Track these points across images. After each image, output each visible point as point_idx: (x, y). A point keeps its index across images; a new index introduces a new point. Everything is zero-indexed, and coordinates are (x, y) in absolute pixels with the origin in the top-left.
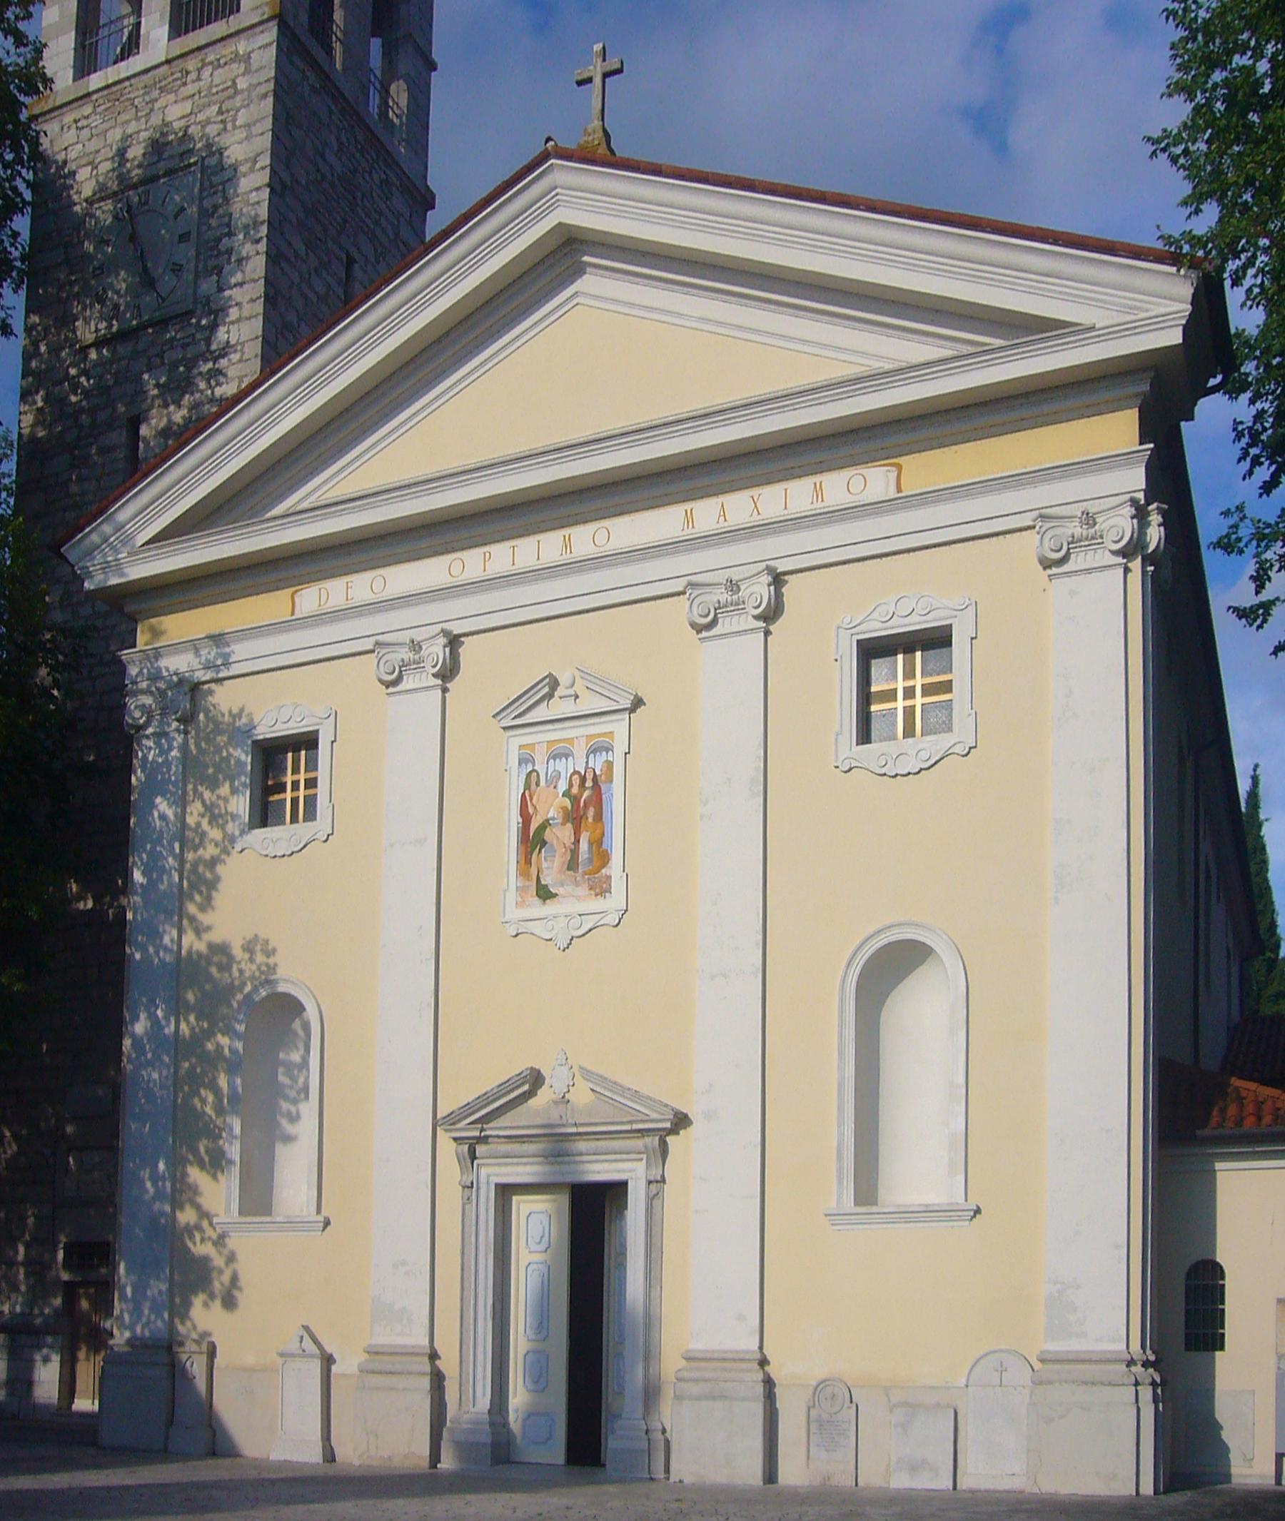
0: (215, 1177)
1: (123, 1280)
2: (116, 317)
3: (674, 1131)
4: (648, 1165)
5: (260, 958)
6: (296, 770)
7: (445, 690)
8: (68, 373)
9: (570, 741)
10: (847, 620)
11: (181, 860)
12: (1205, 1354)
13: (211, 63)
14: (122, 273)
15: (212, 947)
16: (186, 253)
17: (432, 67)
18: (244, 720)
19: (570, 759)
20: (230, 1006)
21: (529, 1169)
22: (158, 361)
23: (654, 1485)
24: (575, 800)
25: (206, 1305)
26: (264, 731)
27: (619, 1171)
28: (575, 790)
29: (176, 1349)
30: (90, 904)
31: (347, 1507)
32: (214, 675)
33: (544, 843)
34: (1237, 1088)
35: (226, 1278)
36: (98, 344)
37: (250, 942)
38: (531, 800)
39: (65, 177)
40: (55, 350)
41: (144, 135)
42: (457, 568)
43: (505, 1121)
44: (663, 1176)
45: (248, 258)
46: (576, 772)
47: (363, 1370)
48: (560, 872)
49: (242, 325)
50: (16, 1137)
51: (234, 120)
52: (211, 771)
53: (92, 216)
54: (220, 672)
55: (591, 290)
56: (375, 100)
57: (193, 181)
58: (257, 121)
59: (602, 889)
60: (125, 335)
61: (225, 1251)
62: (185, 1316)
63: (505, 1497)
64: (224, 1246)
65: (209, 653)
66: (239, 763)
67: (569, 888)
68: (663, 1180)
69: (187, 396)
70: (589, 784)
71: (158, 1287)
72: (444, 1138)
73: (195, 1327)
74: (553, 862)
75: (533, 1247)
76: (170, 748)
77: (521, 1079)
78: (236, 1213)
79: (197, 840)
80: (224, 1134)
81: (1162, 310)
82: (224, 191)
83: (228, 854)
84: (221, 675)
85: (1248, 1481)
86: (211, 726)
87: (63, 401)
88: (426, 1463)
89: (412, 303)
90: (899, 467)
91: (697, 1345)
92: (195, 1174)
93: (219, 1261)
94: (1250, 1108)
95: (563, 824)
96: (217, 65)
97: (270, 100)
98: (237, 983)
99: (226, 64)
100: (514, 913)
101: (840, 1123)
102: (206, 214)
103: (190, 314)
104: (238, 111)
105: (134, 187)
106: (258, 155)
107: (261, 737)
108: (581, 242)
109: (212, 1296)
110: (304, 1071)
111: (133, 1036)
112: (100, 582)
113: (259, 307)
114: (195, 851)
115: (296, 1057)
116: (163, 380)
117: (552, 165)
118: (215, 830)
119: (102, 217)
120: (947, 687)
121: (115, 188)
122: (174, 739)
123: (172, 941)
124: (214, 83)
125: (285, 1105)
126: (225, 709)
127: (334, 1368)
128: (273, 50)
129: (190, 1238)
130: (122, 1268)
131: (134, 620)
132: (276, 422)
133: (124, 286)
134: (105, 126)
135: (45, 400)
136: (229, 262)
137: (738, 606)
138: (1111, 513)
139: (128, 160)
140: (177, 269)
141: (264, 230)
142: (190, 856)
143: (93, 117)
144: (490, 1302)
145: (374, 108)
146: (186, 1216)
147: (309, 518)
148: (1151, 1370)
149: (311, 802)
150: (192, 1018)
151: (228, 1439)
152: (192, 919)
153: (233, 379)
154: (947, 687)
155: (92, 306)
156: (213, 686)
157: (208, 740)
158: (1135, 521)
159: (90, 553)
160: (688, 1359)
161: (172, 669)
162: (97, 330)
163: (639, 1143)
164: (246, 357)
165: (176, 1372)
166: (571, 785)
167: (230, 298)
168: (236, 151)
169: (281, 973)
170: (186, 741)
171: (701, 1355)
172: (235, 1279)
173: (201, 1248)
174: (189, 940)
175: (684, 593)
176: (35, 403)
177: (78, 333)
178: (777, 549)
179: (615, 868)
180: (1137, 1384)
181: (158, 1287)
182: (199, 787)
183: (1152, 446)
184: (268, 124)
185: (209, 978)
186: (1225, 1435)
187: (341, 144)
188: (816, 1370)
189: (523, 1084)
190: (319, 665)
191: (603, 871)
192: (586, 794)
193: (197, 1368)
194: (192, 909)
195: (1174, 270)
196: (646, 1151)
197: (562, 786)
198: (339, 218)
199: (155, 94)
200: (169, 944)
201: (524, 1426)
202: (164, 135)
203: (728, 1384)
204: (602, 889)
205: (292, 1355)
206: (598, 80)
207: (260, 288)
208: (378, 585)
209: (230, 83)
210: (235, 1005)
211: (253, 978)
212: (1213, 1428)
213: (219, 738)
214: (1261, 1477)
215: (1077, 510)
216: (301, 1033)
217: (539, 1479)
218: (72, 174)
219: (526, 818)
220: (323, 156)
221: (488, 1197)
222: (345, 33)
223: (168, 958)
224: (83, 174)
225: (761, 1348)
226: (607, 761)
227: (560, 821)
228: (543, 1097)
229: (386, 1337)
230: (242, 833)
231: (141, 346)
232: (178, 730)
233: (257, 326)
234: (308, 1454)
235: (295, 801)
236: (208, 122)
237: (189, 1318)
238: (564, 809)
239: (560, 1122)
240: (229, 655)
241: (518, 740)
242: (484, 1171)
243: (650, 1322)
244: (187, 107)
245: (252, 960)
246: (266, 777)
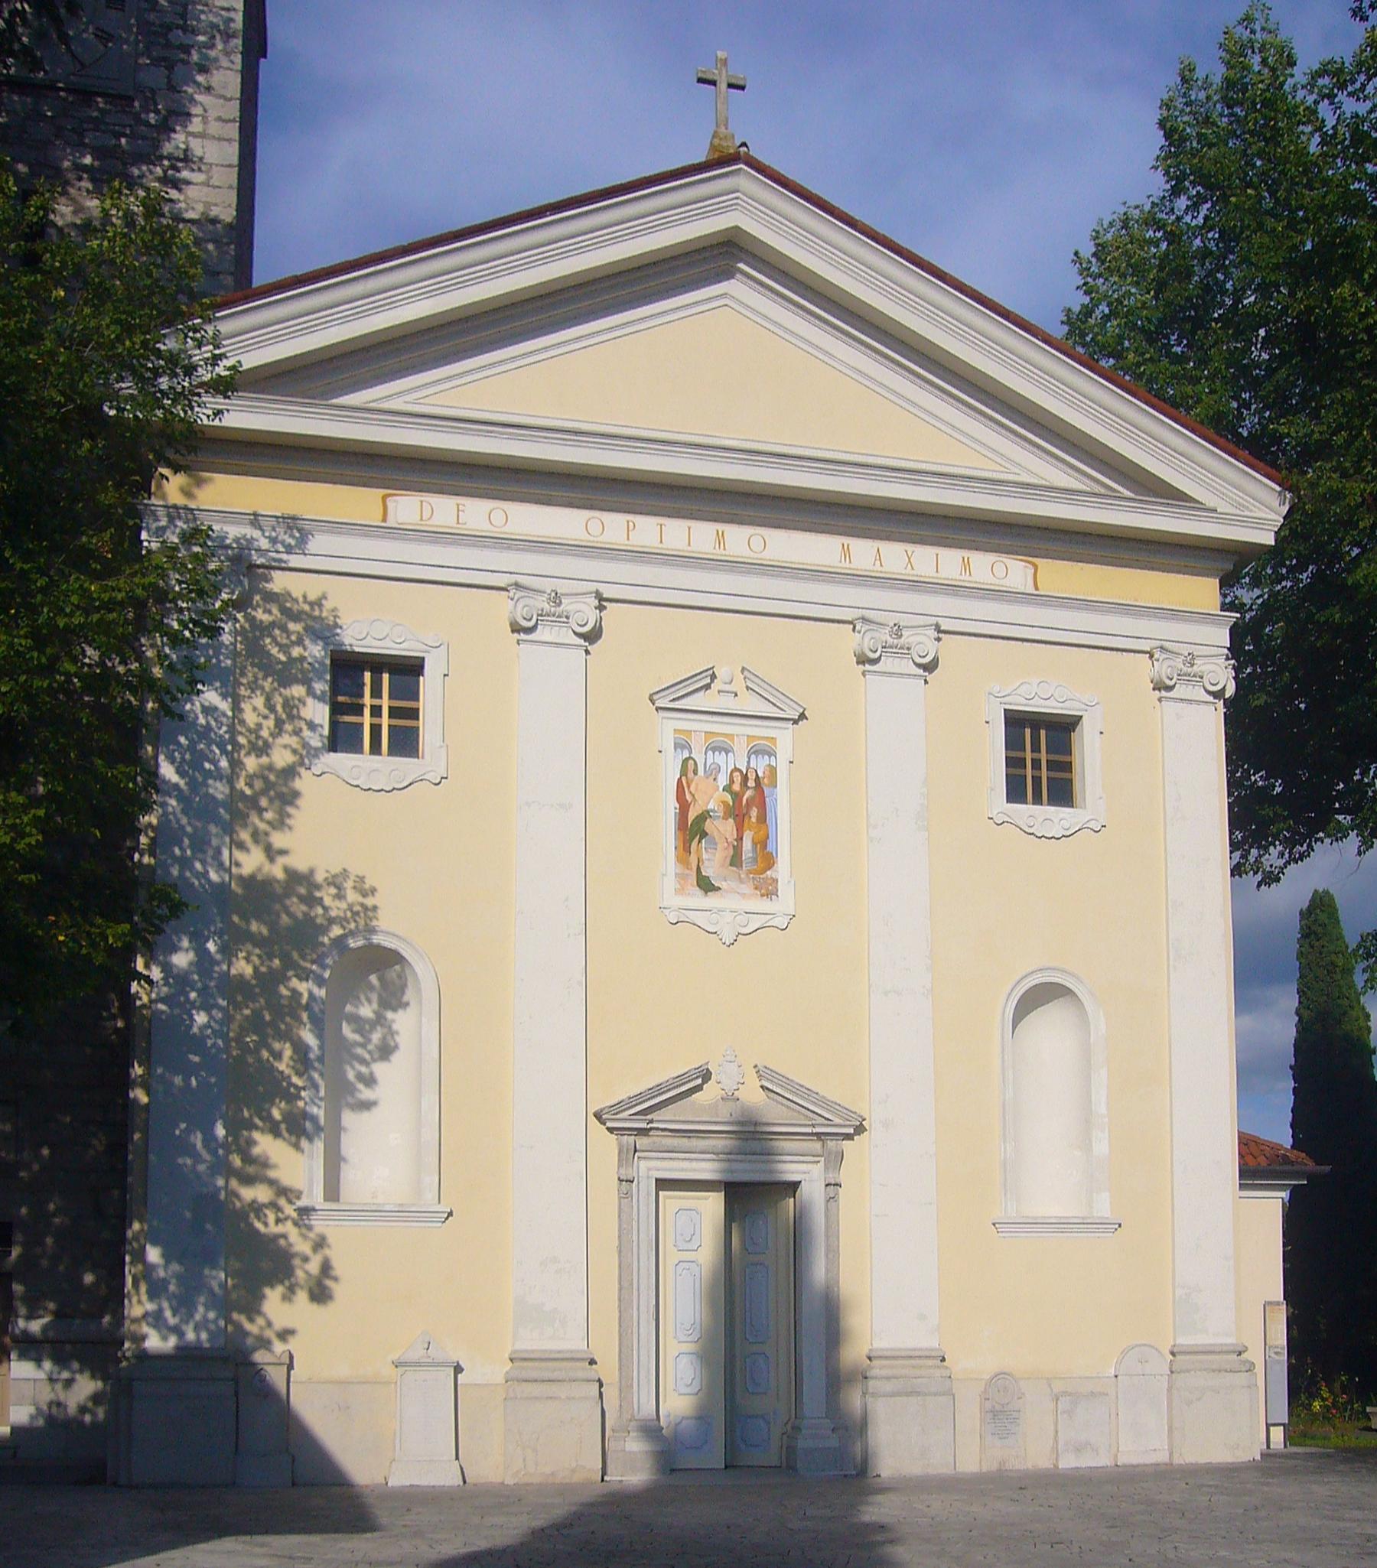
0: (297, 1146)
4: (826, 1168)
5: (352, 896)
9: (731, 736)
15: (295, 877)
19: (730, 754)
24: (736, 797)
28: (736, 787)
33: (704, 834)
35: (314, 1267)
38: (689, 787)
46: (736, 769)
48: (723, 866)
59: (769, 890)
64: (310, 1228)
67: (733, 884)
70: (751, 783)
73: (269, 1324)
74: (714, 854)
81: (1264, 516)
89: (903, 292)
92: (265, 1144)
95: (725, 818)
108: (741, 249)
117: (740, 169)
129: (259, 1219)
132: (392, 305)
138: (919, 630)
147: (447, 427)
164: (214, 182)
166: (732, 781)
171: (888, 1354)
172: (326, 1268)
179: (782, 871)
183: (1238, 615)
189: (697, 1078)
190: (796, 621)
191: (768, 873)
192: (748, 794)
195: (1278, 488)
197: (723, 780)
203: (919, 1380)
204: (769, 890)
215: (1185, 650)
219: (684, 806)
228: (710, 1093)
229: (533, 1341)
237: (259, 1312)
238: (725, 803)
241: (668, 727)
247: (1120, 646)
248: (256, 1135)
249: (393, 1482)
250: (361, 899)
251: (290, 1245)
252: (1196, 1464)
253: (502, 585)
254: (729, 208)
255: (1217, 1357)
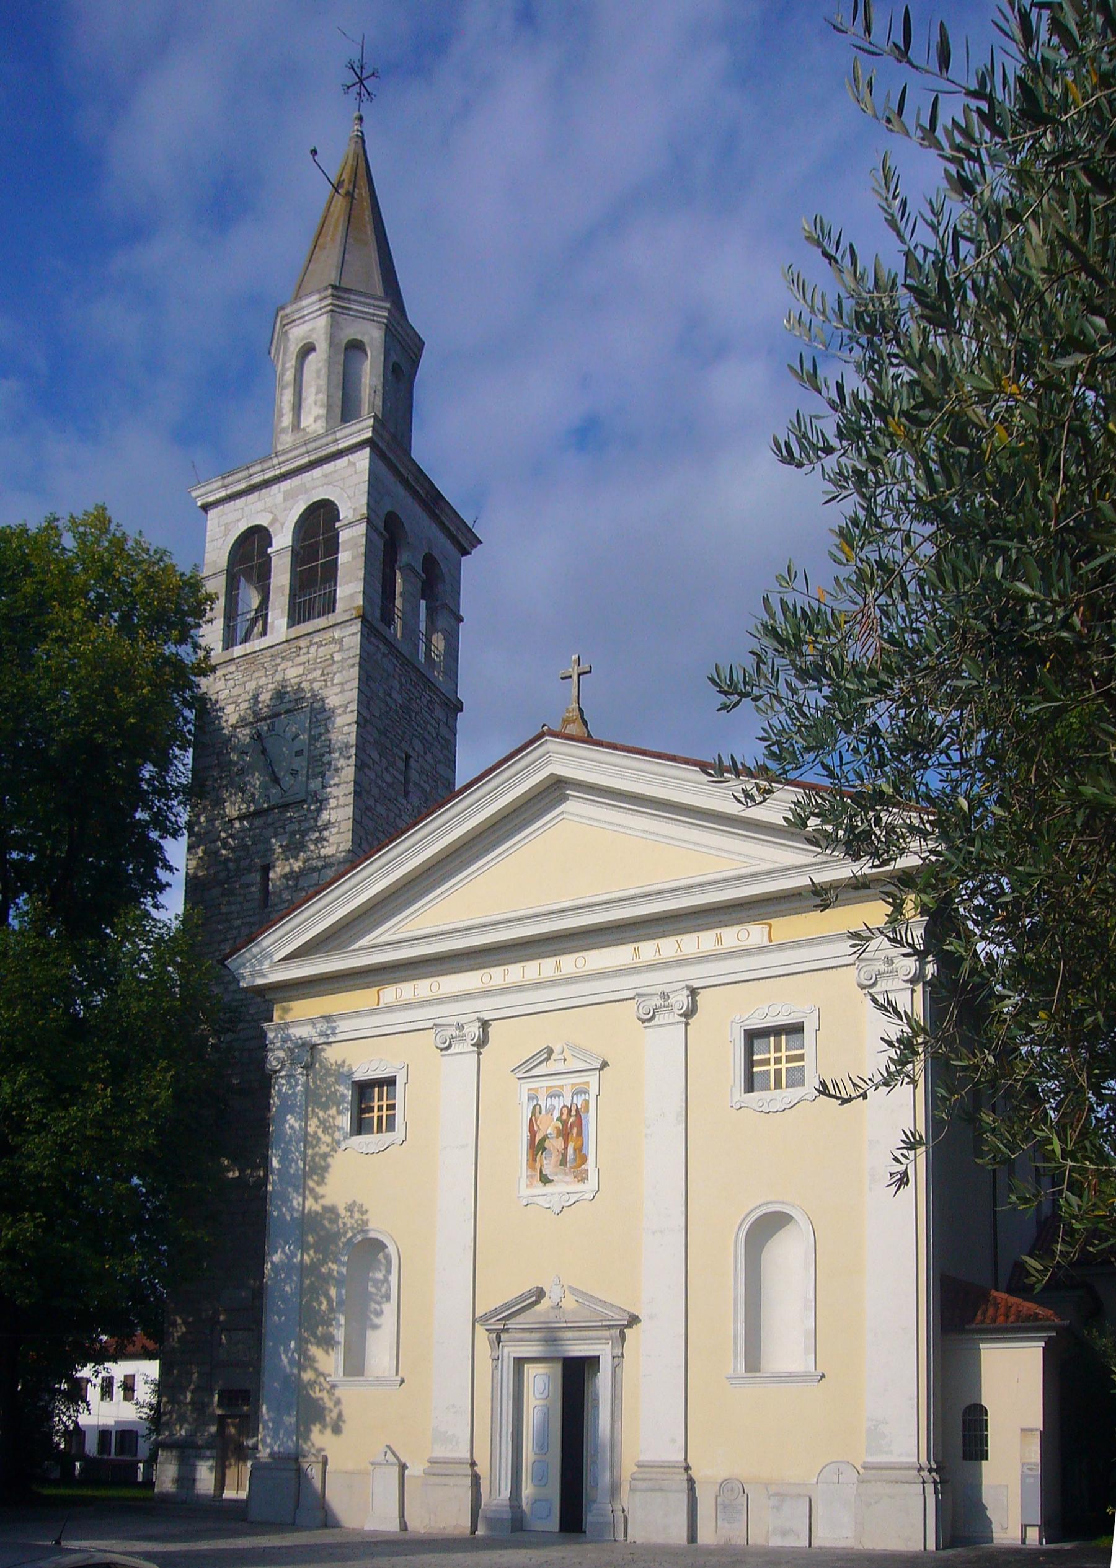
0: (327, 1352)
1: (266, 1417)
2: (253, 801)
3: (629, 1325)
4: (613, 1347)
5: (357, 1216)
6: (380, 1099)
7: (479, 1054)
8: (219, 836)
9: (561, 1087)
10: (738, 1018)
11: (305, 1153)
12: (973, 1462)
13: (316, 643)
14: (257, 774)
15: (324, 1207)
16: (300, 763)
17: (460, 619)
18: (346, 1069)
20: (337, 1246)
21: (535, 1348)
22: (282, 830)
23: (617, 1544)
24: (564, 1123)
25: (321, 1432)
26: (359, 1076)
27: (594, 1350)
28: (564, 1117)
29: (301, 1460)
30: (237, 1174)
31: (383, 1562)
32: (326, 1040)
33: (544, 1149)
34: (995, 1298)
35: (334, 1415)
36: (241, 818)
37: (350, 1205)
39: (217, 711)
40: (211, 821)
41: (271, 686)
42: (486, 979)
43: (521, 1318)
44: (622, 1354)
45: (342, 768)
46: (564, 1106)
47: (427, 1473)
49: (338, 810)
50: (185, 1322)
51: (332, 680)
52: (324, 1099)
53: (236, 737)
54: (330, 1037)
55: (571, 810)
56: (422, 647)
57: (304, 718)
58: (347, 682)
59: (583, 1178)
60: (258, 813)
61: (334, 1398)
62: (307, 1438)
63: (523, 1552)
64: (333, 1394)
65: (322, 1026)
66: (343, 1096)
68: (622, 1356)
69: (302, 854)
70: (573, 1113)
71: (290, 1420)
72: (480, 1331)
73: (313, 1445)
75: (538, 1396)
76: (297, 1085)
77: (531, 1293)
78: (342, 1374)
79: (314, 1142)
80: (334, 1323)
82: (326, 725)
83: (336, 1151)
84: (330, 1040)
85: (1004, 1542)
86: (324, 1071)
87: (217, 853)
88: (468, 1531)
90: (770, 926)
91: (646, 1457)
92: (314, 1350)
93: (329, 1404)
94: (1002, 1310)
95: (557, 1137)
96: (320, 644)
97: (357, 668)
98: (341, 1231)
99: (326, 644)
100: (525, 1191)
101: (735, 1321)
102: (313, 739)
103: (304, 801)
104: (335, 674)
105: (265, 719)
106: (349, 703)
107: (357, 1079)
108: (566, 783)
109: (324, 1426)
110: (385, 1285)
111: (273, 1263)
112: (249, 982)
113: (350, 799)
114: (313, 1149)
115: (380, 1276)
116: (284, 844)
118: (327, 1136)
119: (243, 738)
120: (801, 1057)
121: (251, 720)
122: (299, 1079)
123: (299, 1204)
124: (319, 656)
125: (373, 1306)
126: (333, 1061)
127: (407, 1472)
128: (359, 636)
130: (264, 1408)
131: (272, 1002)
132: (366, 889)
133: (258, 782)
134: (245, 679)
135: (204, 852)
136: (329, 770)
137: (669, 1008)
139: (259, 702)
140: (294, 773)
141: (353, 751)
142: (310, 1152)
143: (236, 674)
144: (510, 1430)
145: (422, 658)
146: (308, 1376)
148: (934, 1474)
149: (391, 1119)
150: (312, 1252)
151: (334, 1516)
152: (312, 1190)
153: (333, 844)
154: (801, 1057)
155: (236, 794)
156: (324, 1046)
157: (322, 1080)
158: (917, 963)
159: (243, 965)
160: (639, 1466)
161: (298, 1036)
162: (240, 809)
163: (607, 1333)
164: (341, 831)
165: (300, 1474)
166: (562, 1114)
167: (330, 793)
168: (333, 700)
169: (371, 1226)
170: (307, 1081)
171: (647, 1464)
172: (340, 1415)
173: (316, 1394)
174: (310, 1203)
175: (634, 998)
176: (197, 854)
177: (227, 810)
178: (695, 974)
180: (924, 1482)
181: (290, 1420)
182: (316, 1110)
183: (927, 918)
184: (356, 684)
185: (324, 1227)
186: (989, 1513)
187: (402, 685)
188: (721, 1472)
192: (572, 1119)
193: (314, 1472)
194: (311, 1183)
196: (611, 1338)
197: (556, 1114)
198: (399, 732)
199: (279, 660)
200: (297, 1207)
201: (532, 1508)
202: (284, 687)
203: (666, 1482)
204: (583, 1178)
205: (380, 1464)
206: (575, 677)
207: (351, 787)
208: (435, 987)
209: (329, 657)
210: (341, 1245)
211: (352, 1228)
212: (980, 1508)
213: (329, 1079)
214: (1013, 1539)
216: (383, 1261)
217: (542, 1540)
218: (222, 709)
220: (390, 695)
221: (509, 1367)
222: (403, 613)
223: (296, 1215)
224: (229, 709)
225: (686, 1459)
226: (585, 1100)
227: (554, 1135)
228: (545, 1304)
229: (440, 1453)
230: (345, 1138)
231: (270, 821)
232: (301, 1074)
233: (350, 811)
234: (391, 1526)
235: (380, 1118)
236: (314, 680)
238: (557, 1128)
239: (555, 1320)
240: (335, 1028)
242: (506, 1350)
243: (614, 1443)
244: (300, 670)
245: (352, 1217)
246: (361, 1102)
247: (781, 973)
248: (309, 1346)
249: (366, 1528)
250: (360, 1217)
251: (324, 1403)
252: (874, 1550)
253: (632, 996)
254: (548, 763)
255: (898, 1472)
